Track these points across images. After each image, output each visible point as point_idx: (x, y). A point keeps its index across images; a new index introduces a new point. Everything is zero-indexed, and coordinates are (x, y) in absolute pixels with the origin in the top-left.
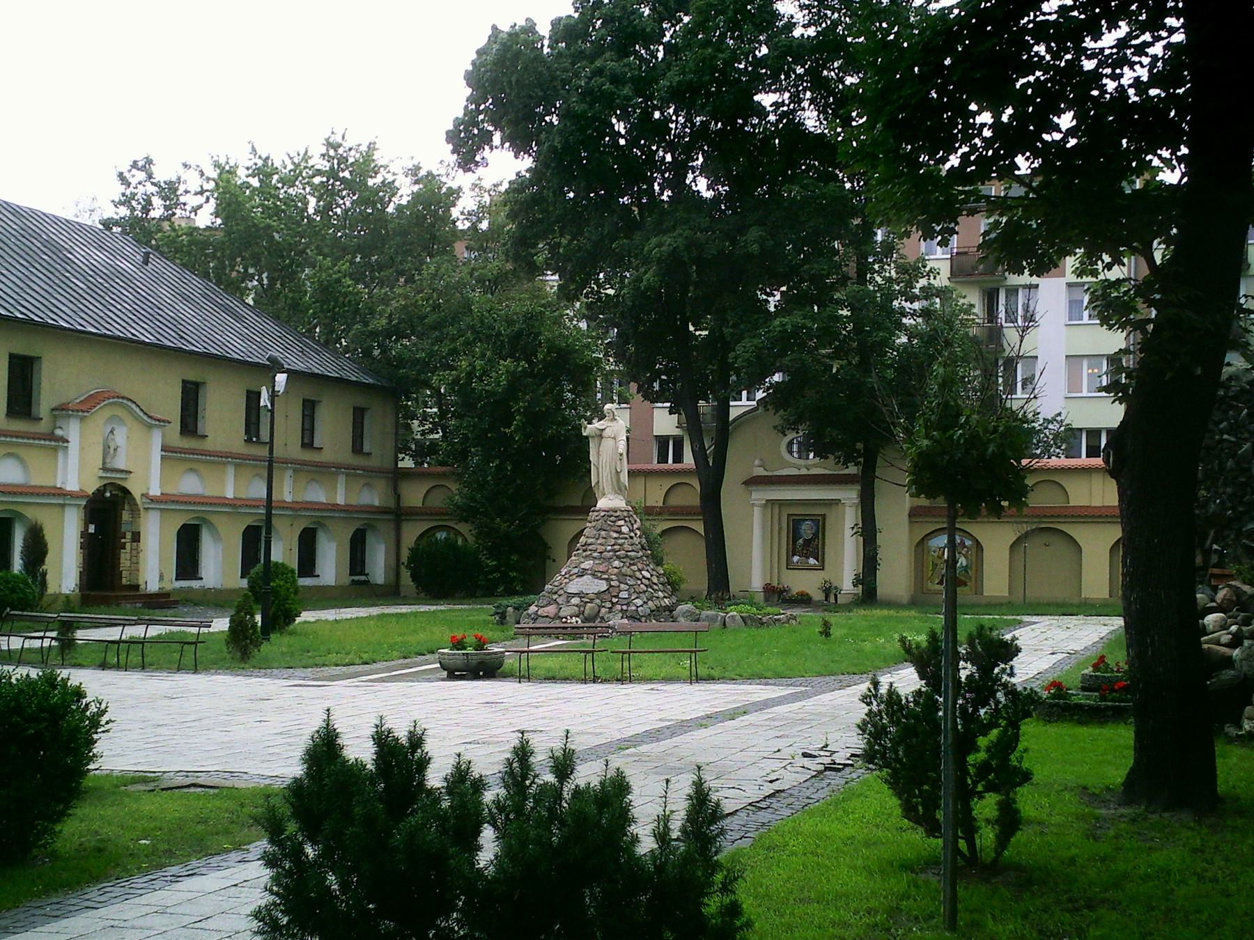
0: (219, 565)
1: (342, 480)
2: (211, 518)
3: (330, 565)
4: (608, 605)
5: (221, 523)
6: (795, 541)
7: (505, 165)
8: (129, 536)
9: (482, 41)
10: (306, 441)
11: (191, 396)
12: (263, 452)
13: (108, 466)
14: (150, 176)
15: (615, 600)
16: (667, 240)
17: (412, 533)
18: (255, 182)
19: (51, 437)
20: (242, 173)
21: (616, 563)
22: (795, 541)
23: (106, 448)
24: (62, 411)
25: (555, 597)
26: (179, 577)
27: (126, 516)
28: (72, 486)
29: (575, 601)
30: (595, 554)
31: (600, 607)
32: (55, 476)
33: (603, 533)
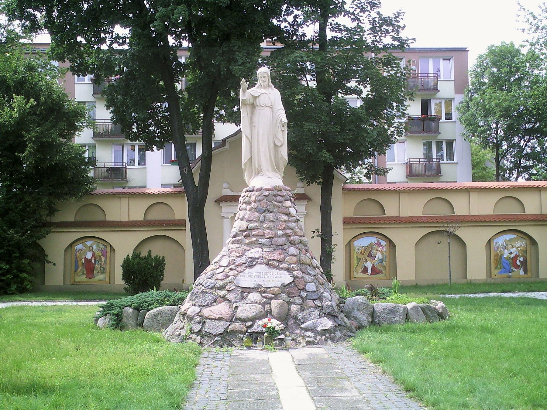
4: (298, 300)
15: (304, 294)
21: (292, 250)
25: (222, 293)
29: (254, 296)
30: (263, 241)
31: (289, 303)
33: (270, 216)
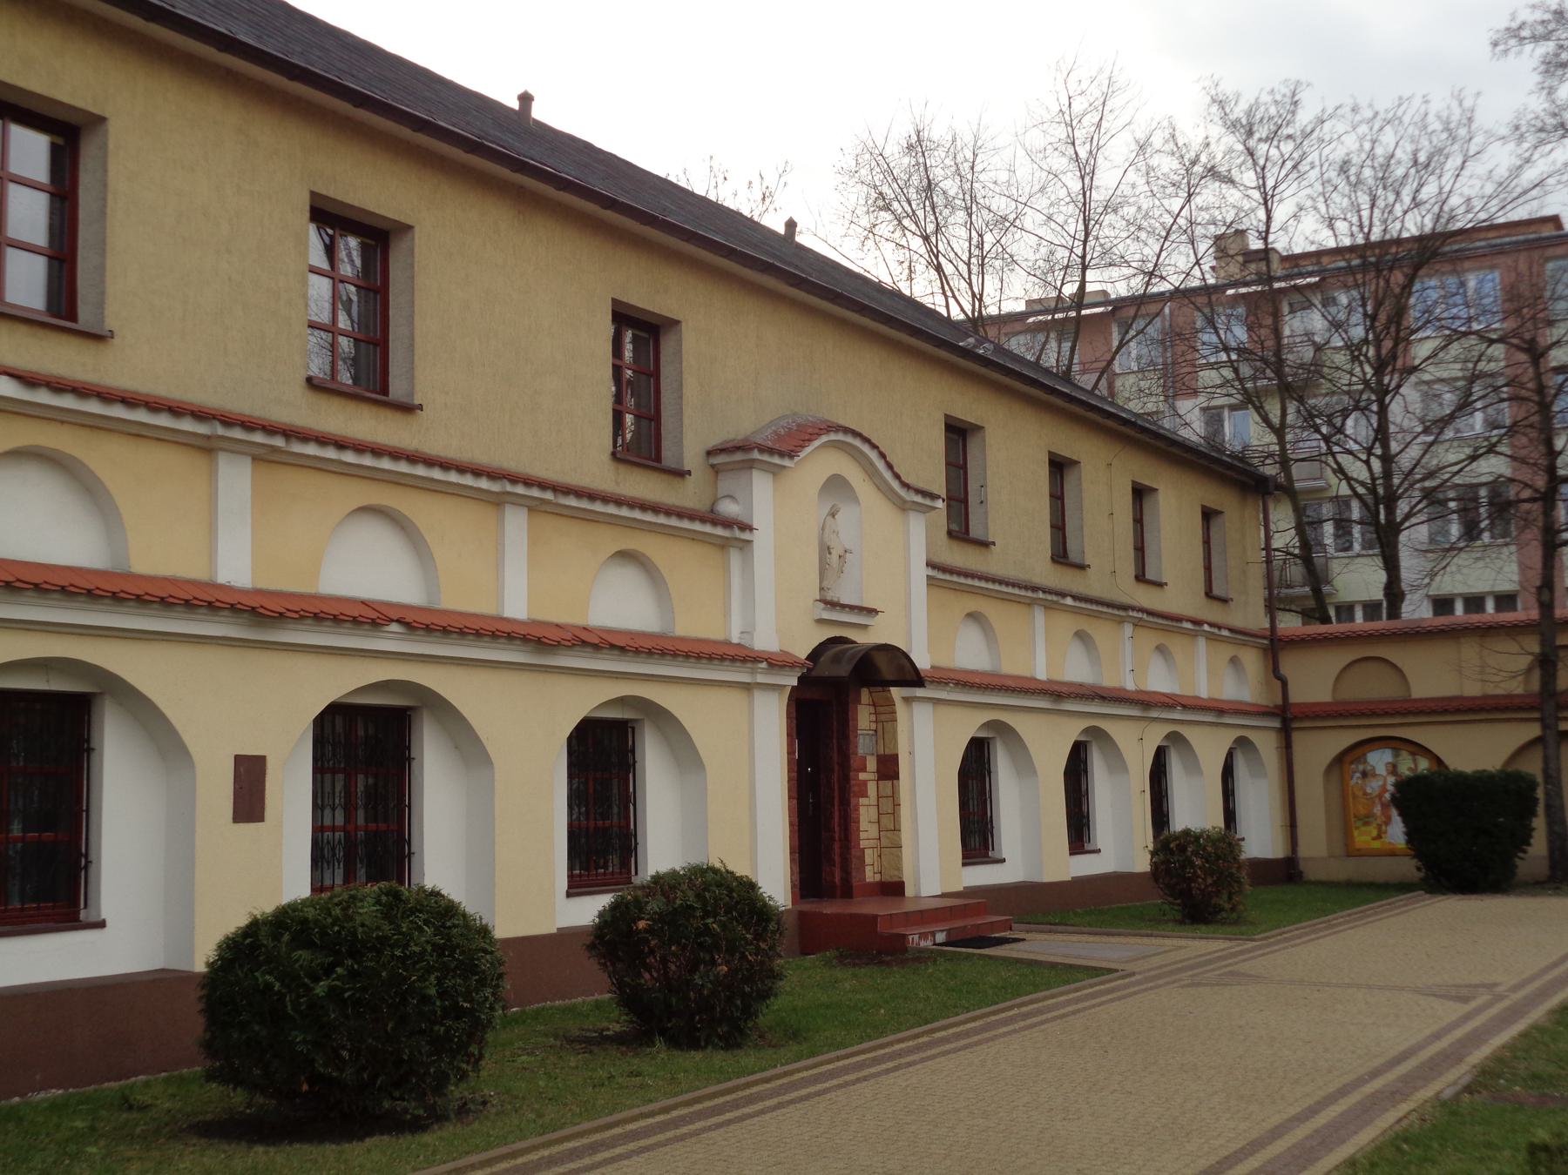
2: (1186, 732)
5: (699, 709)
8: (872, 764)
10: (954, 527)
13: (830, 596)
23: (825, 549)
24: (735, 456)
28: (766, 640)
32: (727, 613)
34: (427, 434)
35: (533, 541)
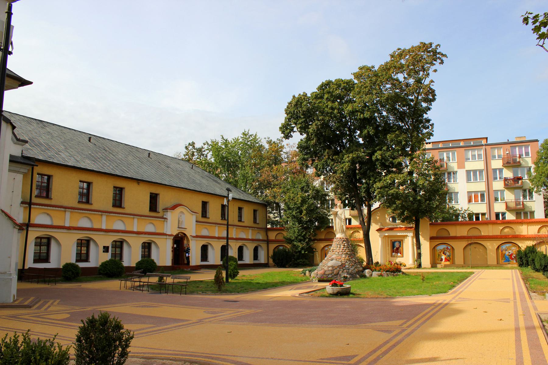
0: (214, 257)
1: (250, 231)
3: (248, 258)
4: (342, 270)
6: (393, 248)
7: (297, 137)
9: (290, 99)
11: (204, 205)
12: (225, 222)
14: (194, 147)
16: (351, 155)
17: (272, 247)
18: (223, 147)
19: (162, 218)
20: (220, 144)
22: (393, 248)
23: (179, 221)
24: (166, 209)
26: (202, 260)
27: (185, 242)
34: (127, 211)
35: (71, 218)
